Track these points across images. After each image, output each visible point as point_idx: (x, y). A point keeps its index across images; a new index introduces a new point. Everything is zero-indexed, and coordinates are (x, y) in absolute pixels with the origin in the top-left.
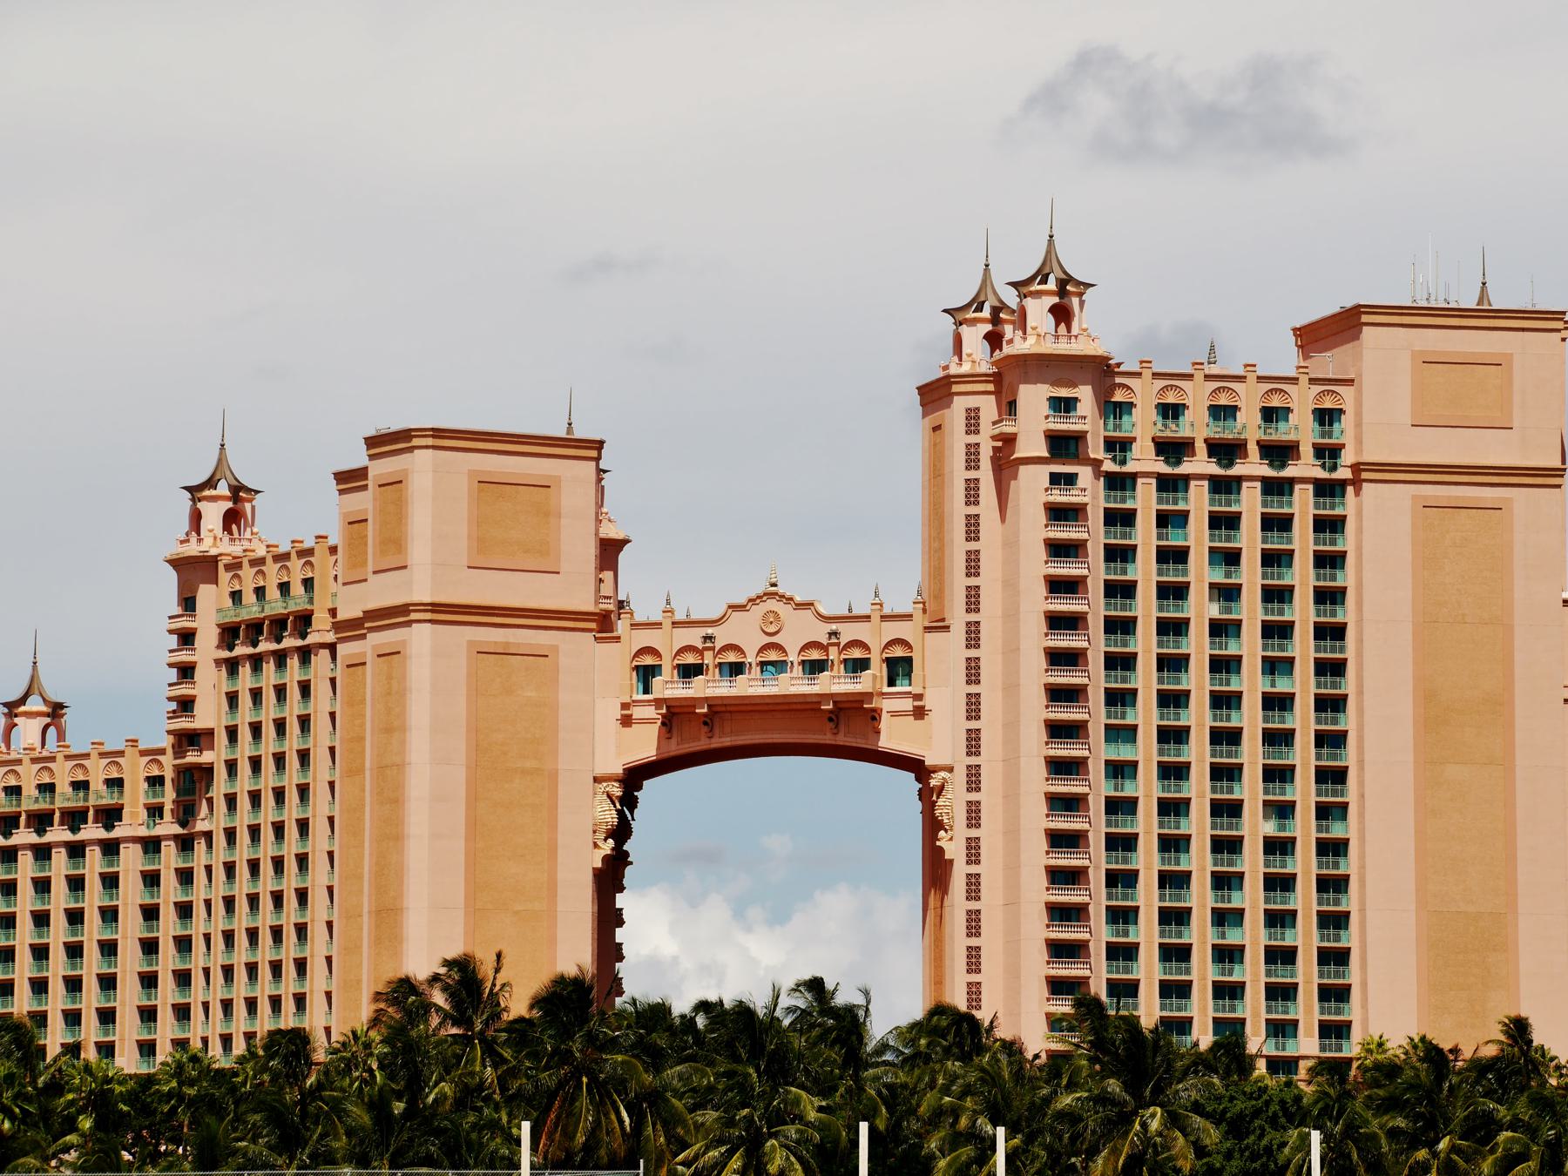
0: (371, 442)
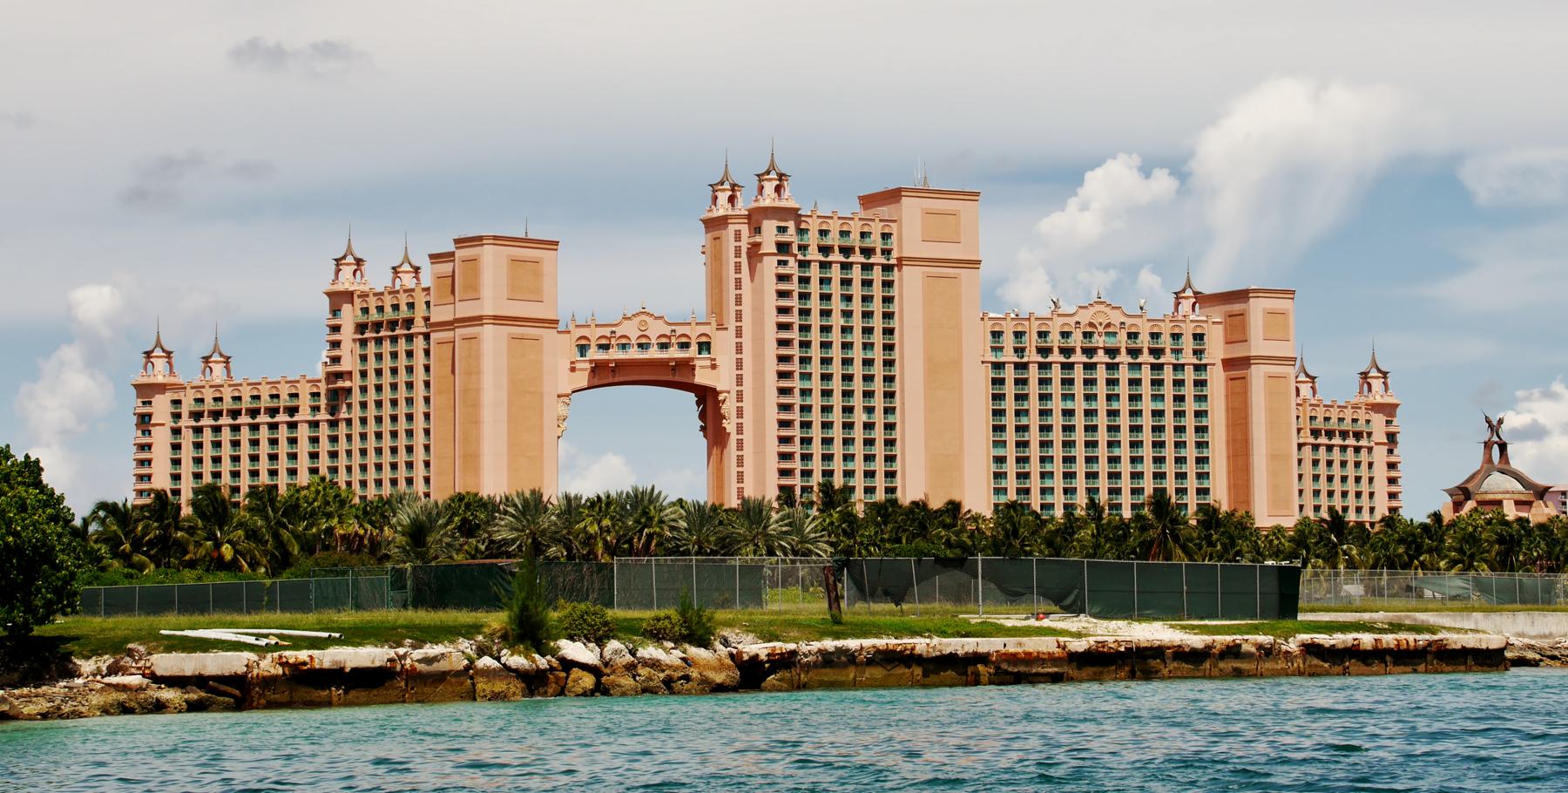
0: (457, 241)
